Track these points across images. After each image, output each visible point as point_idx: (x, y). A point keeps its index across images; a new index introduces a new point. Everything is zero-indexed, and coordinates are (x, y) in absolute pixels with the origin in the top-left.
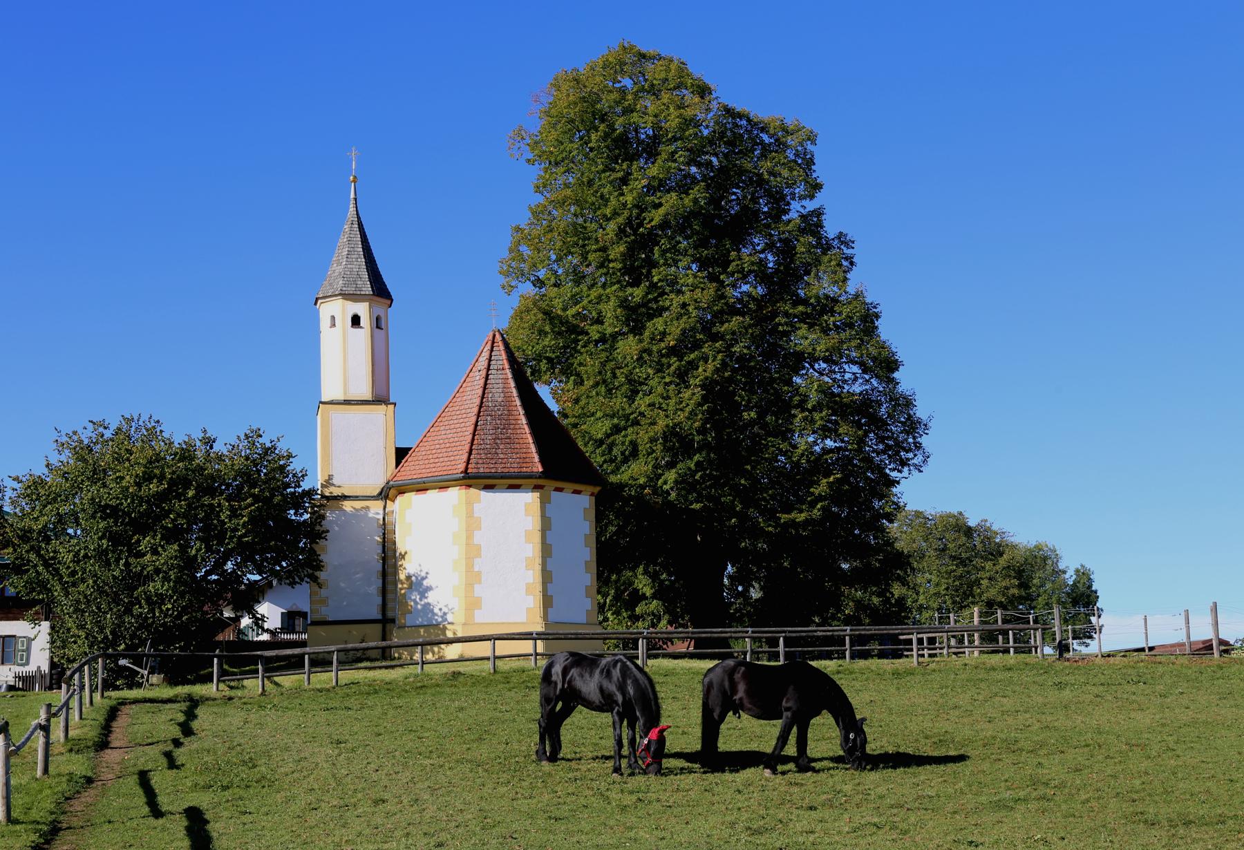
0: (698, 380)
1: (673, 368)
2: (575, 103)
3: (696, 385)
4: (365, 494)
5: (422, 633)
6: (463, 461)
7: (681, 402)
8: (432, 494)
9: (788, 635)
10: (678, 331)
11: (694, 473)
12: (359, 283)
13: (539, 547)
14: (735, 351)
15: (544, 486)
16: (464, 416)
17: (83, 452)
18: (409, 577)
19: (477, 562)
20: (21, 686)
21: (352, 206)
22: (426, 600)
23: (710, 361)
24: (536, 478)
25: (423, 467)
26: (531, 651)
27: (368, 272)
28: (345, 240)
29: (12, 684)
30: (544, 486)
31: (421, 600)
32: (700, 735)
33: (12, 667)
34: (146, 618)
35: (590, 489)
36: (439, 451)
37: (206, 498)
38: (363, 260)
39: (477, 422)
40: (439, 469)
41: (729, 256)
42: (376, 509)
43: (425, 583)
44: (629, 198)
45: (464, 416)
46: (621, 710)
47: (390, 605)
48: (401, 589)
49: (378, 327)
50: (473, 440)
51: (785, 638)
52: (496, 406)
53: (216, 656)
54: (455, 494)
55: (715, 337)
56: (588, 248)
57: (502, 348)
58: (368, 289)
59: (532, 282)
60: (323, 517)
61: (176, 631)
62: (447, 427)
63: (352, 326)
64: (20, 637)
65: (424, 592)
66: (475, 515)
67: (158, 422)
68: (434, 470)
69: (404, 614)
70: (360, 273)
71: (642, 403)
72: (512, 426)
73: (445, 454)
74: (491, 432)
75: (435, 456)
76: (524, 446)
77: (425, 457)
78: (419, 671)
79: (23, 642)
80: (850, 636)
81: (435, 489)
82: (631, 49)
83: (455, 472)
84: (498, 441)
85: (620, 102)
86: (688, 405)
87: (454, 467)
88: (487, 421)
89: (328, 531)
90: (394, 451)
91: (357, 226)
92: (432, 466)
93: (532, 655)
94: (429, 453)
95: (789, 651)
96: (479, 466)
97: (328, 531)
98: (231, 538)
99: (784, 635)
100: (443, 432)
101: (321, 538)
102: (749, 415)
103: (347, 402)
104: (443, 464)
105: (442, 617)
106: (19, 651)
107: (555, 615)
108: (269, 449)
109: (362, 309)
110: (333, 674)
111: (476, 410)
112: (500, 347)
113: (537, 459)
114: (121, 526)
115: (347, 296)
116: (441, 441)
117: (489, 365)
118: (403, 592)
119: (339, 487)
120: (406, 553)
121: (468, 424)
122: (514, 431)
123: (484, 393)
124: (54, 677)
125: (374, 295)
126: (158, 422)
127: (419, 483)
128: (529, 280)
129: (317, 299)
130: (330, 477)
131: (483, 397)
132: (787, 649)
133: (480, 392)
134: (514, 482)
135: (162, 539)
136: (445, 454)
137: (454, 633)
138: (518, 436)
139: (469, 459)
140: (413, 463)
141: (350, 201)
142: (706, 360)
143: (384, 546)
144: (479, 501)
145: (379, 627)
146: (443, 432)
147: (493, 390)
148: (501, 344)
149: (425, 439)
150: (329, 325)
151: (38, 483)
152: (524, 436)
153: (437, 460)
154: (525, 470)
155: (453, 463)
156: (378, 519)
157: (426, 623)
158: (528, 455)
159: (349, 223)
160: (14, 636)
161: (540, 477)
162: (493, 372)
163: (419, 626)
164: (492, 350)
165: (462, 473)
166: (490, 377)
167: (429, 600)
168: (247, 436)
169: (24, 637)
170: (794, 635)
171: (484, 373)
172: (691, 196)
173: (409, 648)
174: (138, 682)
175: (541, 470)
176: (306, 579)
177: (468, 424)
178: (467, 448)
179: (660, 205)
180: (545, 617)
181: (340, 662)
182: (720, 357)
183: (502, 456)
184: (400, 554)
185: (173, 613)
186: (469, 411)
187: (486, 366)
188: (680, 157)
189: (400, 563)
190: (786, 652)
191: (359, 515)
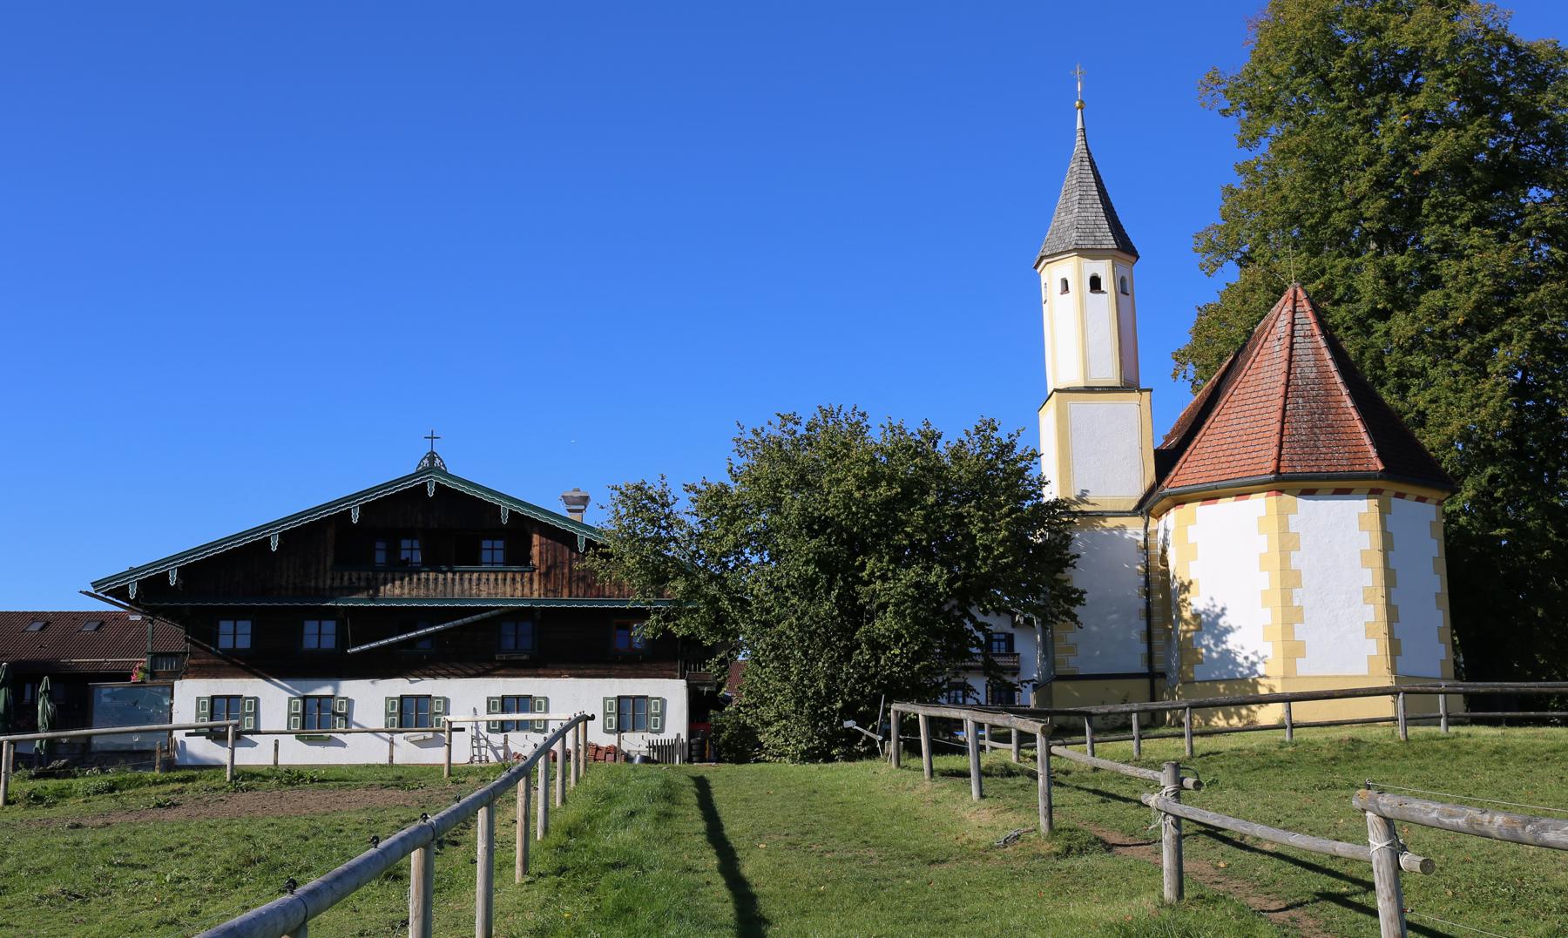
3: (1497, 373)
5: (1222, 690)
7: (1480, 396)
8: (1226, 506)
10: (1471, 304)
12: (1098, 234)
13: (1380, 573)
15: (1383, 490)
17: (774, 451)
18: (1196, 616)
20: (656, 758)
22: (1224, 646)
23: (1514, 342)
24: (1375, 479)
25: (1212, 467)
29: (646, 754)
30: (1383, 490)
31: (1216, 645)
33: (645, 734)
34: (867, 668)
36: (1232, 446)
38: (1100, 206)
39: (1285, 405)
40: (1237, 469)
42: (1134, 528)
43: (1221, 622)
44: (1386, 142)
47: (1158, 654)
49: (1124, 292)
50: (1282, 429)
54: (1260, 504)
58: (1110, 242)
60: (1068, 538)
62: (1241, 415)
64: (653, 698)
65: (1221, 634)
66: (1291, 530)
67: (864, 415)
69: (1191, 665)
72: (1333, 411)
75: (1228, 453)
76: (1353, 436)
77: (1213, 455)
78: (1287, 739)
79: (656, 704)
81: (1230, 496)
84: (1317, 431)
87: (1260, 466)
89: (1078, 556)
90: (1152, 453)
91: (1088, 163)
94: (1217, 448)
96: (1294, 463)
97: (1078, 556)
98: (985, 560)
100: (1235, 422)
101: (1067, 565)
103: (1089, 390)
105: (1249, 668)
106: (652, 715)
108: (1007, 446)
109: (1103, 268)
111: (1281, 390)
113: (1373, 453)
114: (835, 545)
115: (1083, 252)
120: (1190, 583)
121: (1271, 409)
124: (694, 747)
126: (864, 415)
127: (1208, 489)
131: (1289, 374)
133: (1285, 366)
134: (1341, 484)
135: (890, 562)
137: (1271, 690)
138: (1342, 424)
139: (1280, 455)
140: (1196, 463)
141: (1076, 132)
143: (1147, 578)
145: (1145, 682)
146: (1235, 422)
148: (1305, 303)
150: (1060, 291)
151: (721, 493)
152: (1351, 423)
153: (1231, 458)
155: (1256, 461)
156: (1138, 541)
157: (1225, 677)
160: (646, 697)
161: (1381, 478)
163: (1215, 681)
164: (1294, 312)
165: (1272, 473)
166: (1296, 346)
167: (1230, 646)
168: (978, 430)
169: (658, 698)
172: (1471, 133)
173: (1202, 710)
174: (858, 751)
177: (1271, 409)
178: (1276, 439)
180: (1393, 669)
181: (1141, 727)
182: (1528, 335)
183: (1324, 450)
184: (1182, 585)
187: (1289, 332)
189: (1183, 597)
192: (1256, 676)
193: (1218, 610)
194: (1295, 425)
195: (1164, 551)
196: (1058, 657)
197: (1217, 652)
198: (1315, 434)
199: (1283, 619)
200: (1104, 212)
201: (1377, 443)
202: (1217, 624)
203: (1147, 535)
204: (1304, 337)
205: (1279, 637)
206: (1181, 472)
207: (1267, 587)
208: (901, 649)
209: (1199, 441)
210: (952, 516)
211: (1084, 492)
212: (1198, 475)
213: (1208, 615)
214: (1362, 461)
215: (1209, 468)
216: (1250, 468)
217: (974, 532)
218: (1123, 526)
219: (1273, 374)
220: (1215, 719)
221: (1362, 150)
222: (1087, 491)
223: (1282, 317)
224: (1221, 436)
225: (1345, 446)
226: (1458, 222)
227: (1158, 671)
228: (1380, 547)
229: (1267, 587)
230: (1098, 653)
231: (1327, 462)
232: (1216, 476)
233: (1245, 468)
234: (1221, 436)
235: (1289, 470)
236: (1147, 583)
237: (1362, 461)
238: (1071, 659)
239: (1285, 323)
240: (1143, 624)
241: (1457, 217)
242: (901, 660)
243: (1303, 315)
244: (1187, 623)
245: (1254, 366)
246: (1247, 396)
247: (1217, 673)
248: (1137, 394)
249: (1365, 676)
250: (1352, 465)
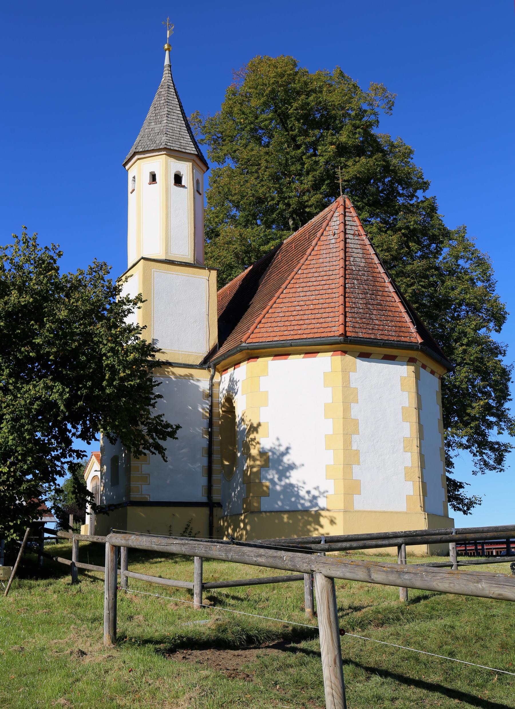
13: (415, 427)
18: (263, 453)
31: (280, 479)
43: (285, 459)
47: (216, 487)
52: (359, 271)
74: (361, 296)
75: (298, 318)
81: (300, 354)
84: (369, 306)
87: (328, 329)
113: (413, 329)
120: (259, 425)
122: (383, 298)
138: (388, 304)
141: (163, 67)
144: (355, 371)
146: (302, 294)
152: (394, 304)
153: (301, 322)
154: (403, 339)
157: (287, 508)
183: (377, 322)
184: (252, 426)
193: (283, 449)
195: (229, 400)
196: (133, 484)
197: (281, 486)
198: (369, 309)
199: (344, 460)
202: (282, 461)
203: (212, 386)
204: (354, 235)
205: (340, 475)
206: (257, 331)
207: (331, 432)
208: (9, 467)
209: (271, 307)
210: (81, 334)
212: (272, 334)
213: (274, 453)
214: (406, 335)
215: (282, 329)
216: (319, 330)
217: (104, 351)
219: (331, 259)
221: (308, 163)
223: (334, 219)
224: (290, 304)
225: (392, 321)
227: (215, 501)
229: (331, 432)
231: (380, 332)
232: (289, 336)
233: (315, 330)
234: (290, 304)
235: (353, 335)
236: (211, 424)
238: (145, 487)
239: (338, 223)
240: (205, 461)
243: (351, 219)
244: (254, 459)
245: (313, 253)
246: (310, 275)
248: (207, 271)
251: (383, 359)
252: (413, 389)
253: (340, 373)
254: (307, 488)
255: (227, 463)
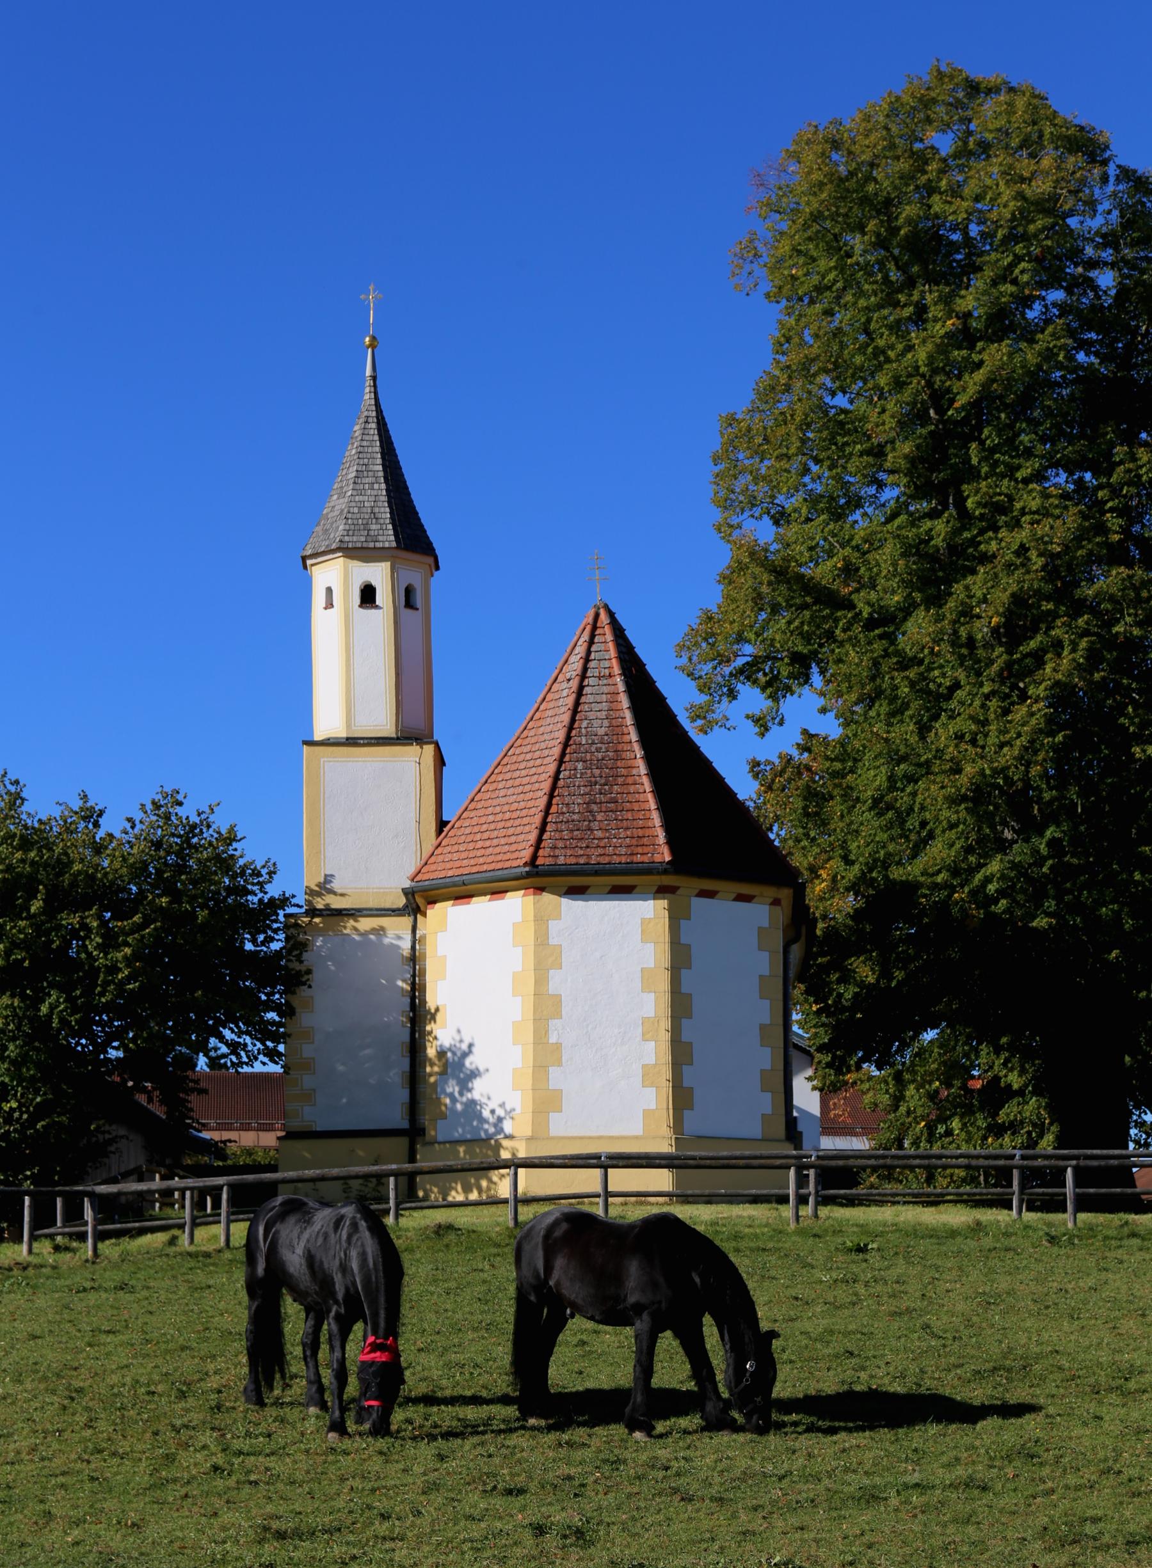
0: (1042, 687)
1: (995, 667)
2: (821, 185)
4: (382, 906)
5: (462, 1154)
6: (530, 843)
8: (481, 906)
9: (1082, 1163)
11: (1040, 861)
12: (374, 527)
13: (666, 999)
14: (1117, 633)
15: (678, 888)
16: (539, 762)
18: (441, 1054)
19: (554, 1024)
21: (367, 390)
22: (469, 1095)
23: (1065, 653)
26: (598, 1188)
27: (390, 506)
28: (354, 452)
30: (678, 888)
31: (461, 1094)
32: (507, 1360)
35: (771, 892)
36: (492, 826)
37: (64, 915)
38: (383, 486)
39: (558, 772)
41: (1112, 455)
42: (398, 932)
43: (468, 1062)
45: (539, 762)
46: (343, 1311)
48: (431, 1075)
50: (549, 805)
51: (1076, 1169)
52: (593, 743)
53: (27, 1193)
55: (1078, 607)
56: (848, 450)
57: (609, 637)
58: (388, 538)
59: (772, 517)
60: (303, 946)
61: (26, 1149)
62: (510, 783)
63: (361, 606)
65: (467, 1078)
67: (17, 782)
68: (481, 860)
70: (376, 510)
71: (943, 732)
72: (620, 780)
73: (503, 832)
75: (486, 835)
77: (470, 838)
80: (1022, 1169)
81: (485, 894)
82: (952, 77)
83: (515, 864)
84: (594, 807)
85: (913, 178)
86: (1019, 735)
88: (576, 770)
91: (374, 426)
92: (479, 853)
93: (598, 1196)
94: (476, 829)
95: (1083, 1194)
96: (557, 852)
98: (106, 983)
99: (1074, 1162)
100: (502, 793)
102: (1144, 751)
104: (498, 850)
105: (495, 1125)
107: (694, 1123)
109: (379, 574)
110: (223, 1225)
112: (607, 635)
113: (661, 837)
116: (498, 809)
117: (585, 669)
118: (432, 1079)
119: (342, 895)
120: (437, 1010)
123: (573, 720)
125: (398, 547)
127: (455, 885)
128: (768, 513)
129: (304, 559)
130: (328, 879)
131: (571, 728)
132: (1077, 1190)
136: (503, 832)
137: (514, 1154)
139: (539, 840)
140: (449, 849)
141: (365, 381)
142: (1058, 645)
144: (558, 917)
147: (591, 715)
149: (471, 806)
152: (642, 797)
153: (488, 843)
154: (639, 858)
157: (469, 1136)
158: (647, 832)
159: (362, 420)
161: (665, 872)
162: (592, 681)
164: (591, 642)
165: (525, 864)
166: (587, 690)
168: (156, 805)
170: (1095, 1163)
171: (574, 684)
175: (668, 858)
176: (261, 1057)
177: (542, 777)
178: (537, 820)
179: (980, 364)
182: (1084, 644)
183: (599, 834)
185: (21, 1115)
186: (546, 752)
187: (579, 671)
188: (1022, 272)
190: (388, 1203)
191: (373, 942)
192: (502, 1136)
194: (567, 800)
197: (462, 1103)
199: (535, 1060)
200: (388, 495)
201: (668, 826)
202: (463, 1065)
204: (599, 678)
211: (328, 879)
212: (448, 866)
213: (454, 1053)
214: (646, 850)
218: (382, 929)
220: (453, 1193)
222: (332, 876)
225: (627, 829)
226: (1019, 475)
228: (667, 964)
230: (344, 1100)
231: (600, 851)
235: (549, 861)
237: (646, 850)
241: (1019, 467)
242: (21, 1115)
247: (460, 1130)
249: (636, 1138)
250: (632, 854)
251: (610, 892)
252: (666, 937)
253: (532, 923)
254: (493, 1105)
255: (859, 1016)
